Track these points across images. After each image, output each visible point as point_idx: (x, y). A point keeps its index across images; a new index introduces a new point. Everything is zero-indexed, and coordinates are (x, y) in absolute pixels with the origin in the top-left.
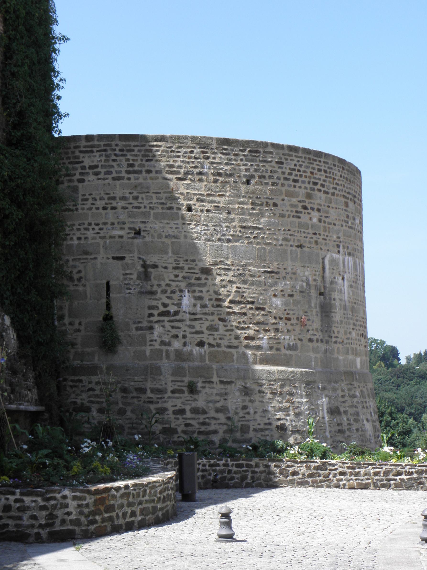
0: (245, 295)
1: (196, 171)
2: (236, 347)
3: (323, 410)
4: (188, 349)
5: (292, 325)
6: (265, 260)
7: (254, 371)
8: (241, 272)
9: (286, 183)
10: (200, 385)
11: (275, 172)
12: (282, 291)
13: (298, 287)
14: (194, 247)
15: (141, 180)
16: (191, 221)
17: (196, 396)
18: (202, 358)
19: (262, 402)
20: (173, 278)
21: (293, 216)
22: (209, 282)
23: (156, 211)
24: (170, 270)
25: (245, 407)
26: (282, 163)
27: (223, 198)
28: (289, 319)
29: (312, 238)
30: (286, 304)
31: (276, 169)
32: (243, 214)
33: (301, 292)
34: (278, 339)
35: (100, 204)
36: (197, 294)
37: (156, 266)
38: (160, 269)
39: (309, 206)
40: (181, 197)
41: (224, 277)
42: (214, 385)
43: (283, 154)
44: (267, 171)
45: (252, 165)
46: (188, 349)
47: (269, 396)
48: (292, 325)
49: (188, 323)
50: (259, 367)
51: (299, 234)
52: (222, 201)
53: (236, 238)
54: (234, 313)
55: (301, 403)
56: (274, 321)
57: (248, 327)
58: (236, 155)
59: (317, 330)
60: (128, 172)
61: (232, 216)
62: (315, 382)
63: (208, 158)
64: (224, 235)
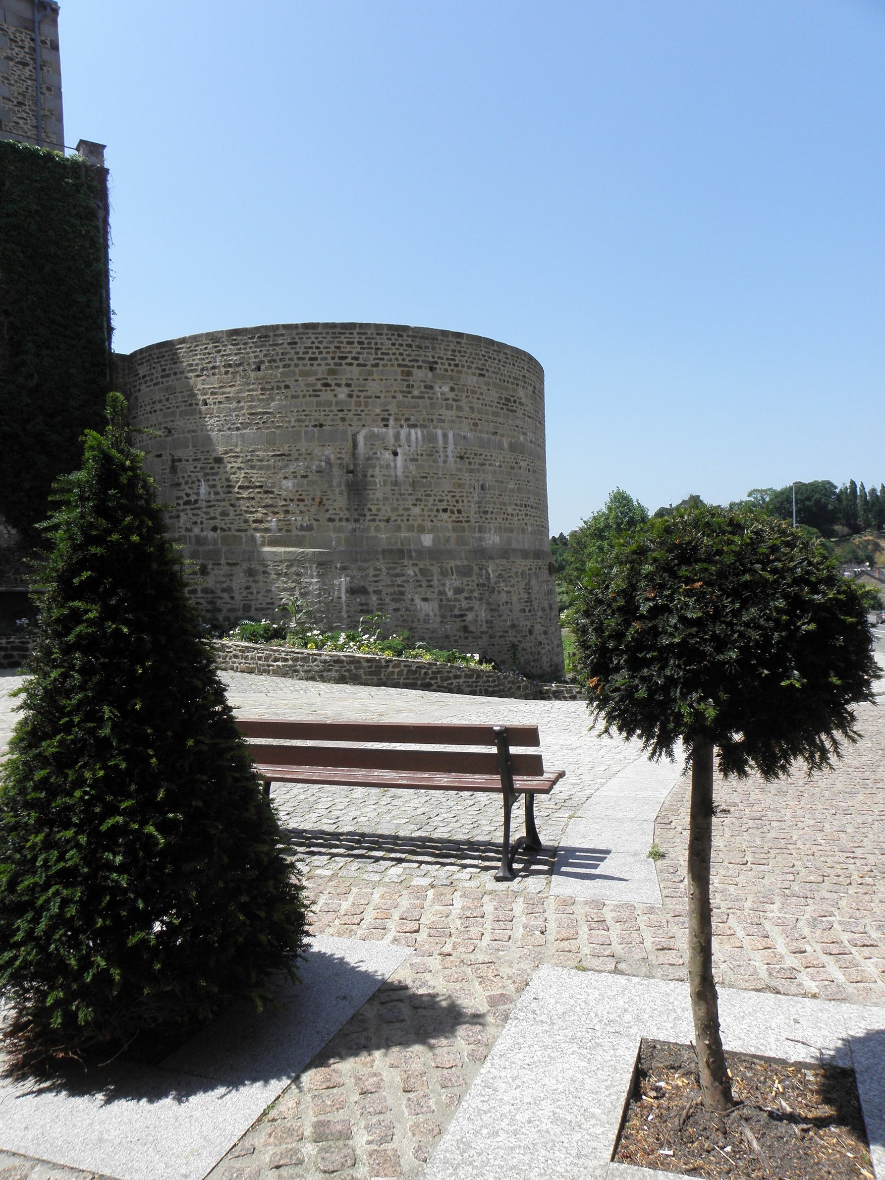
1: (210, 365)
2: (246, 530)
3: (339, 590)
4: (204, 534)
7: (259, 553)
8: (249, 457)
9: (300, 362)
10: (210, 567)
11: (286, 353)
14: (209, 438)
15: (170, 383)
16: (206, 414)
17: (206, 577)
18: (215, 542)
20: (193, 469)
21: (310, 396)
22: (221, 471)
23: (181, 409)
24: (191, 462)
26: (296, 343)
28: (303, 500)
30: (298, 485)
31: (289, 350)
32: (252, 401)
33: (317, 472)
35: (148, 408)
36: (211, 483)
37: (180, 460)
38: (184, 462)
39: (333, 383)
40: (199, 393)
41: (234, 465)
42: (222, 567)
44: (277, 354)
46: (204, 534)
47: (274, 576)
49: (205, 510)
50: (266, 549)
51: (318, 413)
52: (231, 391)
53: (245, 425)
54: (243, 498)
56: (284, 503)
58: (245, 344)
59: (341, 509)
60: (162, 377)
61: (242, 404)
62: (331, 562)
63: (219, 351)
64: (234, 424)
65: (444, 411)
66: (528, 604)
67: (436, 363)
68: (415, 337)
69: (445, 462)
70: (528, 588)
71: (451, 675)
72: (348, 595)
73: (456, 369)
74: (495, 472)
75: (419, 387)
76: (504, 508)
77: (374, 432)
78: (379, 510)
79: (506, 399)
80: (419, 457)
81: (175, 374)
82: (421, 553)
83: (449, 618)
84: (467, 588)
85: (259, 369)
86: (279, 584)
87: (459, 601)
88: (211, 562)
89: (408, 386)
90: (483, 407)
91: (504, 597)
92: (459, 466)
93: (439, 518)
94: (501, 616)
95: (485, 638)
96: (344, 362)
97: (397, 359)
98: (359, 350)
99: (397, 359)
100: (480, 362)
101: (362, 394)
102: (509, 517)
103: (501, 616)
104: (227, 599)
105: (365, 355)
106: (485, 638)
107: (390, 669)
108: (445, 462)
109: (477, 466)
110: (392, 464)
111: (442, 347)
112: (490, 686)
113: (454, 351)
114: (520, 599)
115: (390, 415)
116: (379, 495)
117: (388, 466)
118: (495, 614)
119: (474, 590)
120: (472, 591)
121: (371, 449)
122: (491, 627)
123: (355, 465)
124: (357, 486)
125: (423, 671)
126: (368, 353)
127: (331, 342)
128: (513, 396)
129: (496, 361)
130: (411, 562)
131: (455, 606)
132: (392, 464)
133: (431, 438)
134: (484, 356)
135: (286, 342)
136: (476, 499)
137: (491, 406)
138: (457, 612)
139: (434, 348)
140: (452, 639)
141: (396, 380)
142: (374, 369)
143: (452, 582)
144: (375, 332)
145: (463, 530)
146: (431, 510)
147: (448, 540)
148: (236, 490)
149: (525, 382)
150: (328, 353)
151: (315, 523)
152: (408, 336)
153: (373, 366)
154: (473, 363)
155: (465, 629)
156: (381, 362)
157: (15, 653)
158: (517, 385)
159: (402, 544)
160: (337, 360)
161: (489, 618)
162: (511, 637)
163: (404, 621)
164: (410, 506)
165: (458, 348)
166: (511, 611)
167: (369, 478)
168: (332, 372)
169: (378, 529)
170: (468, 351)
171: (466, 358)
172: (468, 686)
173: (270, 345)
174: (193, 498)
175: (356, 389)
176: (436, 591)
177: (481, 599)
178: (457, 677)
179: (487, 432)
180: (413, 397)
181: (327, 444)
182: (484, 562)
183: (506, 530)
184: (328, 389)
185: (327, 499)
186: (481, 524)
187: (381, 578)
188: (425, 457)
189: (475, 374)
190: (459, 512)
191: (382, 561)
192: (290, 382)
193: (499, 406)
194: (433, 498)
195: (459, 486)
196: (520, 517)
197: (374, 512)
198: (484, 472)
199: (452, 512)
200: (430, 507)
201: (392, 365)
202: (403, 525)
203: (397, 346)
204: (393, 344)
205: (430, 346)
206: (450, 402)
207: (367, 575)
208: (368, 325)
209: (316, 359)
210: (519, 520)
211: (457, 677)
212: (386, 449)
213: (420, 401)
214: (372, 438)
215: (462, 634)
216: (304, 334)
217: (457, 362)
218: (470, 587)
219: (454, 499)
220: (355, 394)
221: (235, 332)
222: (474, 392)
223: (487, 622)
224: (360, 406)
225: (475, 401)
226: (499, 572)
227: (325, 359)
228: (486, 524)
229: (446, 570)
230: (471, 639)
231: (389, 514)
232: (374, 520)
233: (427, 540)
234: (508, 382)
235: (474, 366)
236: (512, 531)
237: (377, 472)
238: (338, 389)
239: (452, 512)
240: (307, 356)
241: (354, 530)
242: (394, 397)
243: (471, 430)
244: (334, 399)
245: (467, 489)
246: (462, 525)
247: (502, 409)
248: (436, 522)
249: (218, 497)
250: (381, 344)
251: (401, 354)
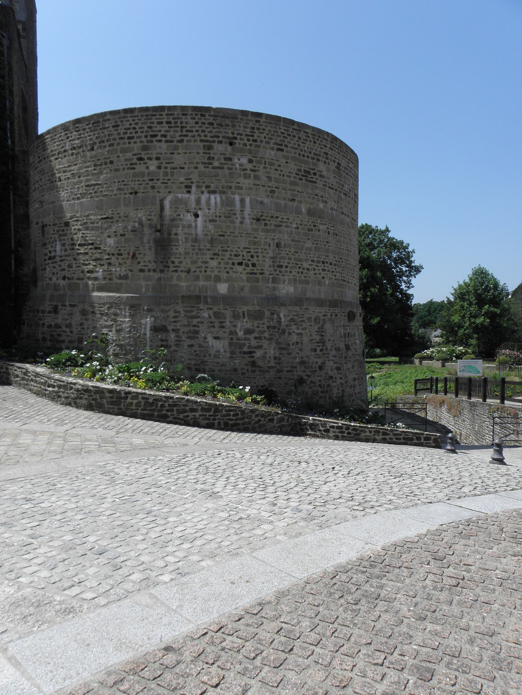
0: (87, 238)
1: (63, 150)
2: (82, 279)
3: (145, 328)
4: (58, 281)
5: (123, 259)
6: (102, 209)
7: (90, 297)
8: (85, 221)
9: (121, 141)
10: (60, 307)
11: (111, 135)
12: (115, 232)
13: (130, 228)
14: (61, 207)
19: (93, 320)
20: (53, 232)
25: (82, 324)
26: (118, 126)
27: (77, 166)
29: (148, 184)
30: (118, 242)
31: (113, 132)
34: (110, 271)
36: (63, 242)
43: (119, 118)
45: (94, 134)
47: (98, 316)
48: (123, 259)
49: (59, 263)
50: (95, 294)
53: (83, 195)
54: (81, 253)
55: (124, 322)
56: (108, 257)
57: (89, 264)
61: (82, 178)
62: (140, 305)
63: (68, 138)
64: (76, 195)
65: (241, 180)
66: (320, 344)
67: (236, 138)
68: (216, 116)
69: (242, 223)
70: (321, 331)
71: (187, 408)
72: (152, 332)
73: (254, 144)
74: (291, 233)
75: (219, 159)
76: (299, 263)
77: (178, 197)
78: (180, 262)
79: (305, 171)
80: (218, 219)
81: (44, 159)
82: (217, 299)
83: (238, 355)
84: (257, 329)
85: (92, 149)
86: (102, 322)
87: (249, 340)
88: (60, 304)
89: (209, 158)
90: (281, 177)
91: (295, 338)
92: (254, 226)
93: (234, 270)
94: (289, 354)
95: (272, 372)
96: (154, 139)
97: (200, 136)
98: (167, 129)
99: (200, 136)
100: (279, 139)
101: (169, 166)
102: (305, 271)
103: (289, 354)
104: (69, 333)
105: (172, 133)
106: (272, 372)
107: (129, 400)
108: (242, 223)
109: (273, 227)
110: (193, 224)
111: (242, 125)
112: (232, 420)
113: (253, 128)
114: (312, 340)
115: (192, 183)
116: (181, 250)
117: (190, 226)
118: (284, 352)
119: (264, 332)
120: (262, 332)
121: (175, 212)
122: (279, 363)
123: (162, 225)
124: (163, 243)
125: (160, 403)
126: (175, 131)
127: (145, 123)
128: (313, 169)
129: (296, 139)
130: (206, 306)
131: (244, 344)
132: (193, 224)
133: (230, 203)
134: (282, 133)
135: (111, 125)
136: (271, 255)
137: (289, 176)
138: (246, 349)
139: (234, 126)
140: (240, 372)
141: (198, 153)
142: (179, 144)
143: (241, 326)
144: (181, 113)
145: (257, 280)
146: (227, 263)
147: (242, 289)
148: (77, 247)
149: (327, 158)
150: (142, 132)
151: (130, 273)
152: (210, 116)
153: (179, 141)
154: (272, 139)
155: (253, 364)
156: (185, 139)
158: (318, 160)
159: (199, 291)
160: (149, 138)
161: (277, 355)
162: (299, 372)
163: (197, 355)
164: (208, 260)
165: (257, 126)
166: (301, 350)
167: (173, 236)
168: (145, 148)
169: (179, 278)
170: (267, 129)
171: (265, 135)
172: (206, 419)
173: (101, 129)
174: (53, 254)
175: (164, 162)
176: (228, 331)
177: (270, 339)
178: (193, 410)
179: (284, 199)
180: (213, 168)
181: (140, 208)
182: (276, 308)
183: (301, 282)
184: (142, 162)
185: (139, 254)
186: (275, 276)
187: (179, 319)
188: (223, 218)
189: (273, 149)
190: (254, 265)
191: (181, 305)
192: (114, 158)
193: (298, 177)
194: (229, 253)
195: (255, 243)
196: (317, 272)
197: (177, 264)
198: (280, 232)
199: (247, 265)
200: (226, 260)
201: (195, 141)
202: (201, 275)
203: (200, 124)
204: (197, 123)
205: (230, 124)
206: (248, 172)
207: (168, 317)
208: (175, 108)
209: (132, 138)
210: (315, 274)
211: (193, 410)
212: (188, 211)
213: (220, 171)
214: (176, 202)
215: (250, 368)
216: (124, 117)
217: (256, 138)
218: (260, 329)
219: (249, 254)
220: (163, 166)
221: (78, 121)
222: (271, 164)
223: (275, 358)
224: (167, 176)
225: (273, 171)
226: (291, 317)
227: (139, 137)
228: (280, 277)
229: (239, 314)
230: (258, 372)
231: (190, 266)
232: (176, 271)
233: (223, 288)
234: (308, 157)
235: (273, 141)
236: (307, 283)
237: (180, 230)
238: (149, 162)
239: (247, 265)
240: (126, 136)
241: (160, 279)
242: (196, 168)
243: (268, 196)
244: (146, 171)
245: (262, 247)
246: (256, 276)
247: (300, 179)
248: (231, 273)
249: (67, 253)
250: (186, 123)
251: (203, 131)
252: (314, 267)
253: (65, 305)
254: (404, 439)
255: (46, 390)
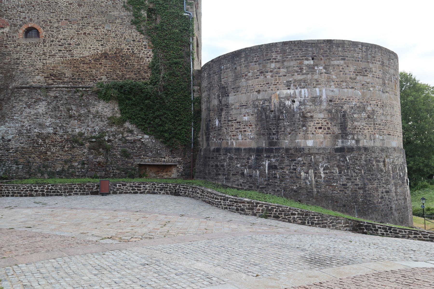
36: (332, 103)
107: (258, 208)
157: (136, 188)
184: (262, 74)
252: (368, 127)
253: (221, 154)
254: (429, 237)
255: (214, 201)
